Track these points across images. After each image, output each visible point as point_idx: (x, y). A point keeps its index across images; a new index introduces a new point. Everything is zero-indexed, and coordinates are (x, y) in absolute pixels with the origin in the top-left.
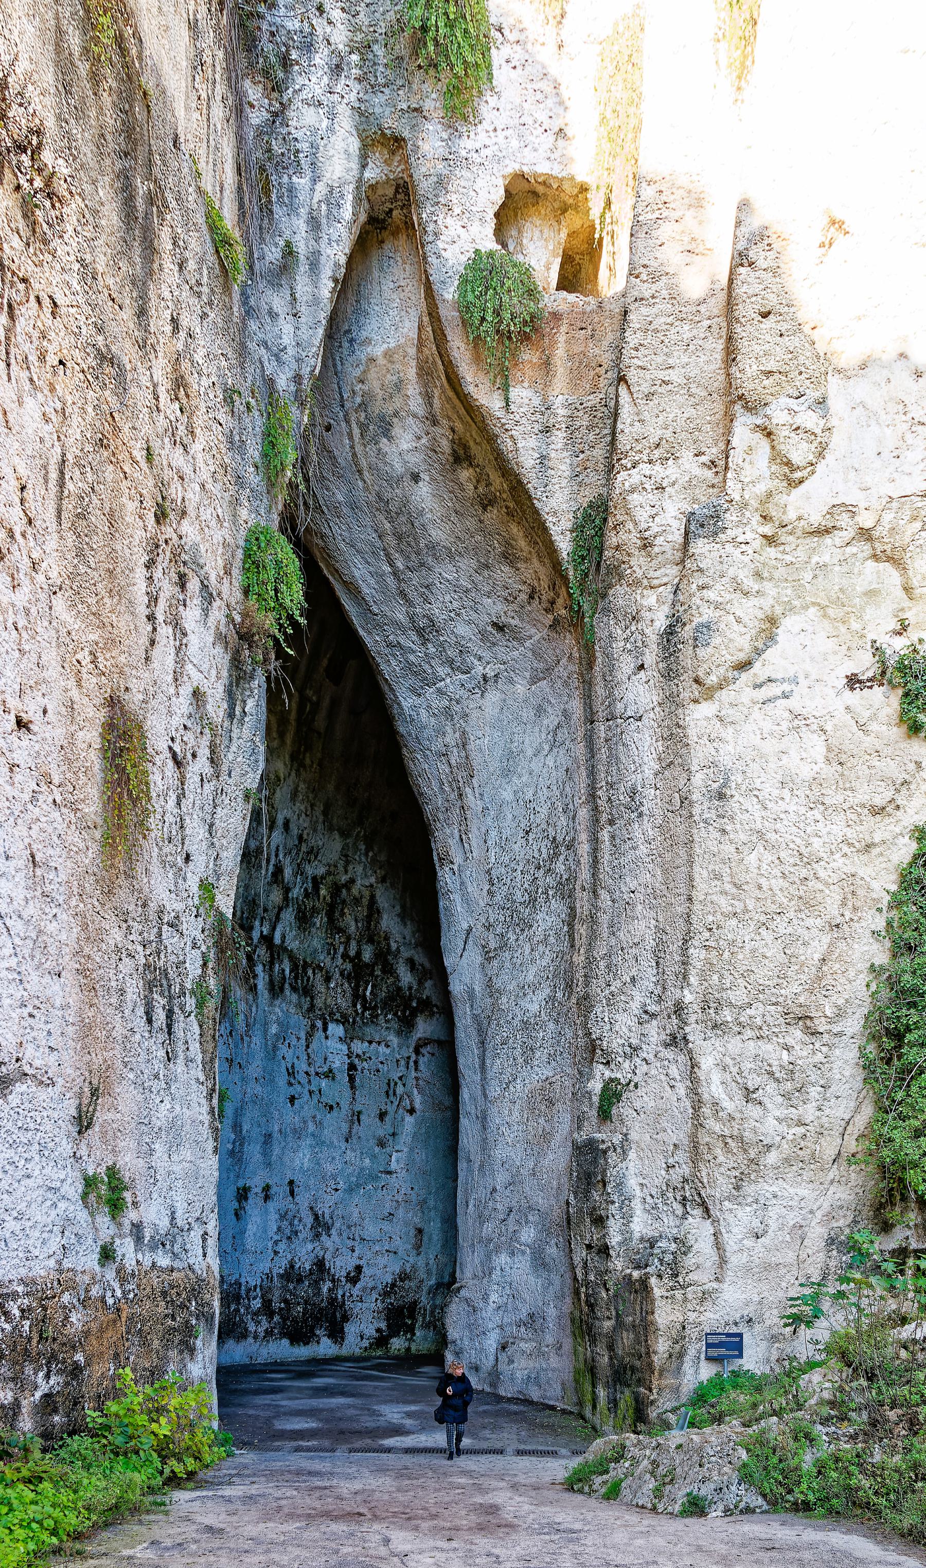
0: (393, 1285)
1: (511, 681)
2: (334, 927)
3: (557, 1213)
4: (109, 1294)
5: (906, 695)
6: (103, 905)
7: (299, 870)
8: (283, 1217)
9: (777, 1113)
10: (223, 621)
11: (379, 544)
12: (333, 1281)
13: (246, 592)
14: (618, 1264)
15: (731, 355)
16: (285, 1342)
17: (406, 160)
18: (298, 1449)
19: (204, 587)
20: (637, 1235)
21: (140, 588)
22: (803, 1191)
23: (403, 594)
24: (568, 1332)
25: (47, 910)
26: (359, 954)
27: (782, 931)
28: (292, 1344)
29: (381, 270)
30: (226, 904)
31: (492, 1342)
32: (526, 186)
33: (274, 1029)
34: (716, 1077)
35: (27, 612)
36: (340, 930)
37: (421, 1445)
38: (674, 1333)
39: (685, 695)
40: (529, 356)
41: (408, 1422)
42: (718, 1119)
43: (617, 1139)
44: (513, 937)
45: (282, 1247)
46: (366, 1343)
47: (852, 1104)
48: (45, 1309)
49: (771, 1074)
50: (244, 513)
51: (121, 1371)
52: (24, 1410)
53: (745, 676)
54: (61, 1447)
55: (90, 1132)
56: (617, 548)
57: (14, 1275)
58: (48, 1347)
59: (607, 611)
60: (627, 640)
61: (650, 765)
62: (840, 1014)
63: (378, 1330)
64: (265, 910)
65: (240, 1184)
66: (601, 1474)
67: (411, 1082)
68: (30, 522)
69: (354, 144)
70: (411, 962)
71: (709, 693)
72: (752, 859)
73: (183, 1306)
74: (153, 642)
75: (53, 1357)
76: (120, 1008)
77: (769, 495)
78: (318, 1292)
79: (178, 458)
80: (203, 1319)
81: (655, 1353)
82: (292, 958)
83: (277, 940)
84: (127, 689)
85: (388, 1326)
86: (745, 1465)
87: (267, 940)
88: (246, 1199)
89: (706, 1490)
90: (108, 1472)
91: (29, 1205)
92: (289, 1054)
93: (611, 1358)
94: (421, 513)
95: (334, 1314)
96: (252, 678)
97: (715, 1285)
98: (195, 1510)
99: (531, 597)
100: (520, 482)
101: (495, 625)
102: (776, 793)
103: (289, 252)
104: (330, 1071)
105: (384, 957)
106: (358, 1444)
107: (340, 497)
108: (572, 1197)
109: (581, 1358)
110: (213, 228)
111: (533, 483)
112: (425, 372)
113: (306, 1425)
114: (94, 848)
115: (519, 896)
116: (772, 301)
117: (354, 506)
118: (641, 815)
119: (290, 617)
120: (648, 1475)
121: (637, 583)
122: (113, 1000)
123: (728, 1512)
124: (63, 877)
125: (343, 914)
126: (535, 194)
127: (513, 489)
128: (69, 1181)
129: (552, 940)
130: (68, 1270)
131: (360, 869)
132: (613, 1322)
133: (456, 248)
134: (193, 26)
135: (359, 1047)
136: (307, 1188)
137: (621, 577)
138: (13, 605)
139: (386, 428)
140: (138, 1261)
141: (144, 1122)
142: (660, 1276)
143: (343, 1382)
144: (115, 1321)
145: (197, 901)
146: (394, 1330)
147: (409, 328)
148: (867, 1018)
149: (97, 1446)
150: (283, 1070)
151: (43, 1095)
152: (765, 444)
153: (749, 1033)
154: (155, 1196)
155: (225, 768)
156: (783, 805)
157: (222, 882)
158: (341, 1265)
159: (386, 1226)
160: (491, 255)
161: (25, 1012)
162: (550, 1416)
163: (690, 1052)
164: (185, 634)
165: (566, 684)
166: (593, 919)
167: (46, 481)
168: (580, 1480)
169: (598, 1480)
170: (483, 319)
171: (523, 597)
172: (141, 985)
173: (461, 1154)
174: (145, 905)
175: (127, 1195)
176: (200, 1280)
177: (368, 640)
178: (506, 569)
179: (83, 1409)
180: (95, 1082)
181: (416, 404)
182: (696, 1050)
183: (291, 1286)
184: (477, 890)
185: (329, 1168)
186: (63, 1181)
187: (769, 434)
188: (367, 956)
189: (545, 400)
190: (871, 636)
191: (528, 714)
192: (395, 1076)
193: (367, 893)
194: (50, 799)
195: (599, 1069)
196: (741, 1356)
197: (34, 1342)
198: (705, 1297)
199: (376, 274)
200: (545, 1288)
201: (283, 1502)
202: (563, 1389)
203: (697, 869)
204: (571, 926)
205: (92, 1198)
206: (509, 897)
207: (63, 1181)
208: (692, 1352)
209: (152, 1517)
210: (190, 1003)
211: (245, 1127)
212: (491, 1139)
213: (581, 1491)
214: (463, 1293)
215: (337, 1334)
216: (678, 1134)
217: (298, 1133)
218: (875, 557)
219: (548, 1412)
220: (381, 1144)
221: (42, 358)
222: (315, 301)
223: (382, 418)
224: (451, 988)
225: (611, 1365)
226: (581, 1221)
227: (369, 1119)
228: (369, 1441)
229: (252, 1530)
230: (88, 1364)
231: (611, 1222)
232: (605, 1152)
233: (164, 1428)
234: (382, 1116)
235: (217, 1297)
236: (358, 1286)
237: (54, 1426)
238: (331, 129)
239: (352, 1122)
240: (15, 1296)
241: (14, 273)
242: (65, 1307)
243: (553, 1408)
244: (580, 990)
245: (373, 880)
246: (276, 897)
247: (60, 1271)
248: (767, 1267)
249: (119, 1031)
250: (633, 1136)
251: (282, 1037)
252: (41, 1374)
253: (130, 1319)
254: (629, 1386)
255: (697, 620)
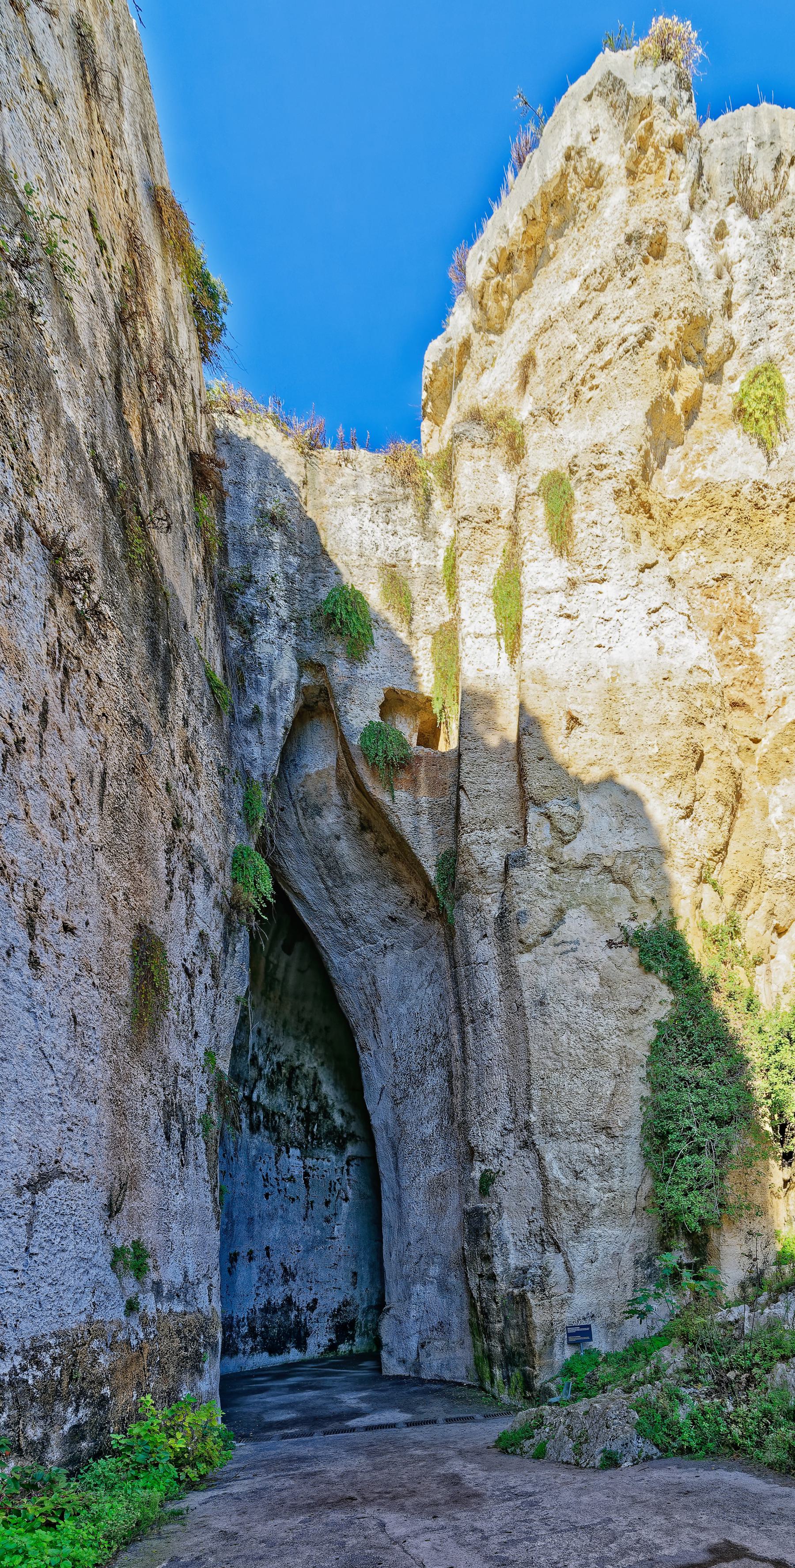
0: (339, 1310)
1: (402, 949)
2: (291, 1091)
3: (454, 1255)
4: (133, 1336)
5: (641, 951)
6: (132, 1058)
7: (268, 1058)
8: (262, 1271)
9: (596, 1185)
10: (220, 895)
11: (316, 872)
12: (298, 1310)
13: (235, 880)
14: (503, 1286)
15: (522, 777)
16: (266, 1354)
17: (325, 676)
18: (285, 1437)
19: (207, 873)
20: (512, 1266)
21: (162, 863)
22: (617, 1232)
23: (333, 901)
24: (468, 1332)
25: (86, 1056)
26: (308, 1107)
27: (586, 1079)
28: (270, 1355)
29: (312, 730)
30: (224, 1065)
31: (414, 1343)
32: (395, 695)
33: (253, 1152)
34: (555, 1165)
35: (74, 858)
36: (296, 1093)
37: (377, 1423)
38: (546, 1327)
39: (513, 949)
40: (403, 775)
41: (363, 1406)
42: (559, 1190)
43: (495, 1206)
44: (412, 1091)
45: (262, 1291)
46: (322, 1350)
47: (640, 1178)
48: (75, 1355)
49: (590, 1162)
50: (232, 838)
51: (142, 1398)
52: (52, 1443)
53: (548, 940)
54: (86, 1471)
55: (119, 1215)
56: (465, 873)
57: (47, 1330)
58: (76, 1387)
59: (461, 907)
60: (474, 922)
61: (496, 989)
62: (627, 1125)
63: (330, 1340)
64: (246, 1081)
65: (232, 1251)
66: (529, 1438)
67: (345, 1182)
68: (78, 802)
69: (295, 665)
70: (342, 1113)
71: (529, 948)
72: (564, 1038)
73: (194, 1340)
74: (171, 898)
75: (83, 1393)
76: (145, 1129)
77: (552, 847)
78: (288, 1318)
79: (188, 795)
80: (209, 1348)
81: (535, 1342)
82: (264, 1109)
83: (255, 1098)
84: (151, 922)
85: (337, 1337)
86: (639, 1424)
87: (248, 1099)
88: (236, 1260)
89: (616, 1447)
90: (129, 1492)
91: (63, 1273)
92: (264, 1167)
93: (503, 1348)
94: (342, 856)
95: (299, 1332)
96: (240, 931)
97: (569, 1295)
98: (208, 1513)
99: (412, 902)
100: (403, 840)
101: (390, 918)
102: (574, 1002)
103: (257, 711)
104: (292, 1177)
105: (324, 1110)
106: (330, 1427)
107: (291, 846)
108: (466, 1245)
109: (480, 1349)
110: (210, 679)
111: (411, 840)
112: (341, 782)
113: (288, 1416)
114: (125, 1020)
115: (414, 1066)
116: (543, 753)
117: (300, 851)
118: (492, 1016)
119: (264, 898)
120: (566, 1438)
121: (479, 891)
122: (140, 1123)
123: (635, 1462)
124: (99, 1034)
125: (297, 1084)
126: (401, 700)
127: (398, 843)
128: (100, 1252)
129: (438, 1091)
130: (98, 1322)
131: (307, 1058)
132: (502, 1324)
133: (358, 720)
134: (196, 581)
135: (310, 1162)
136: (279, 1251)
137: (469, 889)
138: (63, 851)
139: (318, 811)
140: (157, 1310)
141: (164, 1209)
142: (533, 1292)
143: (311, 1379)
144: (138, 1357)
145: (203, 1062)
146: (340, 1340)
147: (330, 761)
148: (642, 1128)
149: (120, 1465)
150: (260, 1177)
151: (79, 1188)
152: (546, 823)
153: (573, 1138)
154: (172, 1261)
155: (222, 982)
156: (579, 1009)
157: (221, 1052)
158: (303, 1299)
159: (333, 1272)
160: (379, 724)
161: (65, 1127)
162: (460, 1391)
163: (537, 1150)
164: (194, 898)
165: (436, 948)
166: (465, 1077)
167: (91, 781)
168: (512, 1445)
169: (528, 1443)
170: (377, 755)
171: (407, 902)
172: (161, 1113)
173: (384, 1223)
174: (165, 1061)
175: (150, 1262)
176: (206, 1319)
177: (310, 925)
178: (396, 887)
179: (109, 1432)
180: (124, 1179)
181: (336, 799)
182: (541, 1149)
183: (269, 1316)
184: (386, 1064)
185: (293, 1237)
186: (94, 1253)
187: (549, 817)
188: (314, 1108)
189: (415, 798)
190: (617, 921)
191: (413, 966)
192: (335, 1179)
193: (312, 1072)
194: (90, 981)
195: (477, 1164)
196: (591, 1340)
197: (65, 1384)
198: (564, 1302)
199: (309, 732)
200: (449, 1305)
201: (285, 1494)
202: (467, 1371)
203: (531, 1044)
204: (450, 1082)
205: (120, 1265)
206: (408, 1068)
207: (94, 1253)
208: (559, 1339)
209: (170, 1528)
210: (198, 1128)
211: (235, 1214)
212: (405, 1213)
213: (514, 1453)
214: (391, 1312)
215: (301, 1345)
216: (533, 1200)
217: (271, 1217)
218: (614, 881)
219: (458, 1388)
220: (327, 1220)
221: (90, 708)
222: (274, 738)
223: (316, 806)
224: (372, 1122)
225: (503, 1353)
226: (473, 1259)
227: (319, 1206)
228: (337, 1424)
229: (263, 1530)
230: (113, 1395)
231: (495, 1259)
232: (487, 1215)
233: (179, 1443)
234: (327, 1203)
235: (220, 1330)
236: (315, 1312)
237: (81, 1451)
238: (280, 655)
239: (308, 1208)
240: (48, 1347)
241: (69, 652)
242: (94, 1351)
243: (461, 1384)
244: (460, 1118)
245: (315, 1064)
246: (253, 1073)
247: (90, 1323)
248: (600, 1281)
249: (144, 1144)
250: (505, 1204)
251: (259, 1157)
252: (70, 1409)
253: (151, 1354)
254: (517, 1366)
255: (517, 910)
